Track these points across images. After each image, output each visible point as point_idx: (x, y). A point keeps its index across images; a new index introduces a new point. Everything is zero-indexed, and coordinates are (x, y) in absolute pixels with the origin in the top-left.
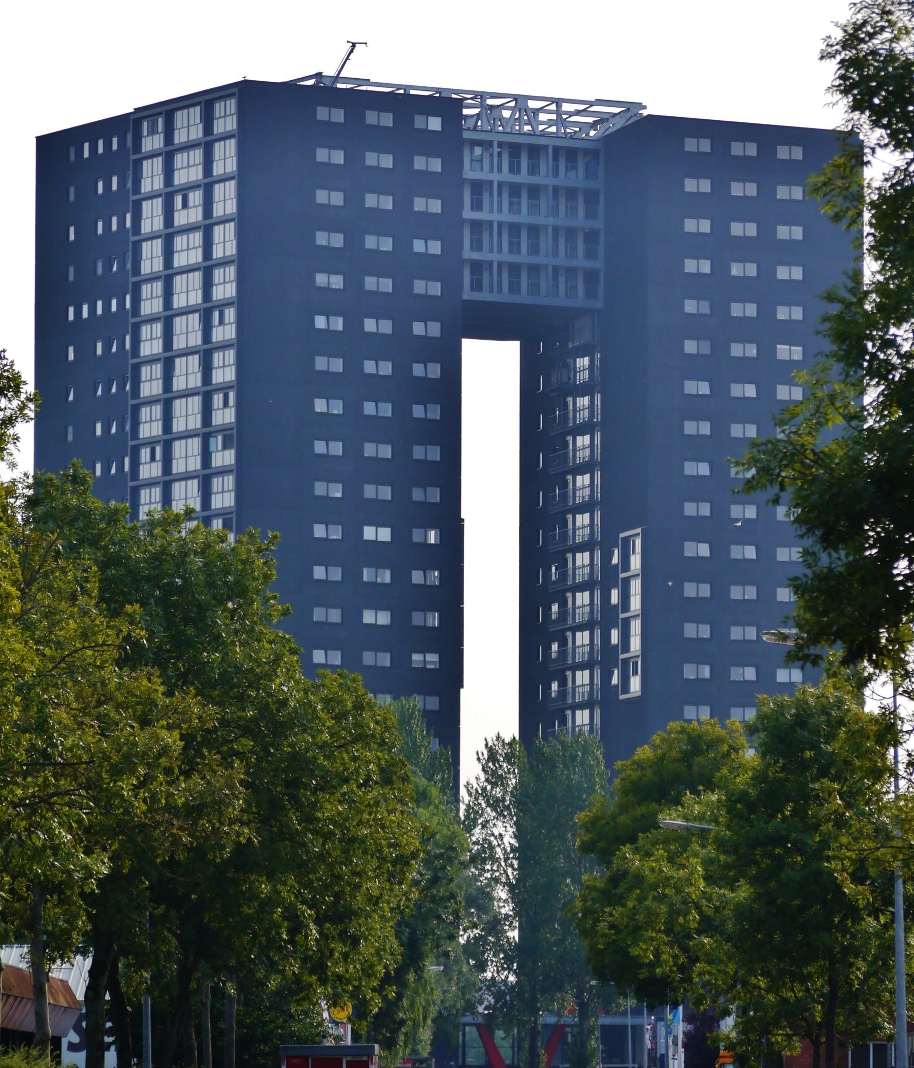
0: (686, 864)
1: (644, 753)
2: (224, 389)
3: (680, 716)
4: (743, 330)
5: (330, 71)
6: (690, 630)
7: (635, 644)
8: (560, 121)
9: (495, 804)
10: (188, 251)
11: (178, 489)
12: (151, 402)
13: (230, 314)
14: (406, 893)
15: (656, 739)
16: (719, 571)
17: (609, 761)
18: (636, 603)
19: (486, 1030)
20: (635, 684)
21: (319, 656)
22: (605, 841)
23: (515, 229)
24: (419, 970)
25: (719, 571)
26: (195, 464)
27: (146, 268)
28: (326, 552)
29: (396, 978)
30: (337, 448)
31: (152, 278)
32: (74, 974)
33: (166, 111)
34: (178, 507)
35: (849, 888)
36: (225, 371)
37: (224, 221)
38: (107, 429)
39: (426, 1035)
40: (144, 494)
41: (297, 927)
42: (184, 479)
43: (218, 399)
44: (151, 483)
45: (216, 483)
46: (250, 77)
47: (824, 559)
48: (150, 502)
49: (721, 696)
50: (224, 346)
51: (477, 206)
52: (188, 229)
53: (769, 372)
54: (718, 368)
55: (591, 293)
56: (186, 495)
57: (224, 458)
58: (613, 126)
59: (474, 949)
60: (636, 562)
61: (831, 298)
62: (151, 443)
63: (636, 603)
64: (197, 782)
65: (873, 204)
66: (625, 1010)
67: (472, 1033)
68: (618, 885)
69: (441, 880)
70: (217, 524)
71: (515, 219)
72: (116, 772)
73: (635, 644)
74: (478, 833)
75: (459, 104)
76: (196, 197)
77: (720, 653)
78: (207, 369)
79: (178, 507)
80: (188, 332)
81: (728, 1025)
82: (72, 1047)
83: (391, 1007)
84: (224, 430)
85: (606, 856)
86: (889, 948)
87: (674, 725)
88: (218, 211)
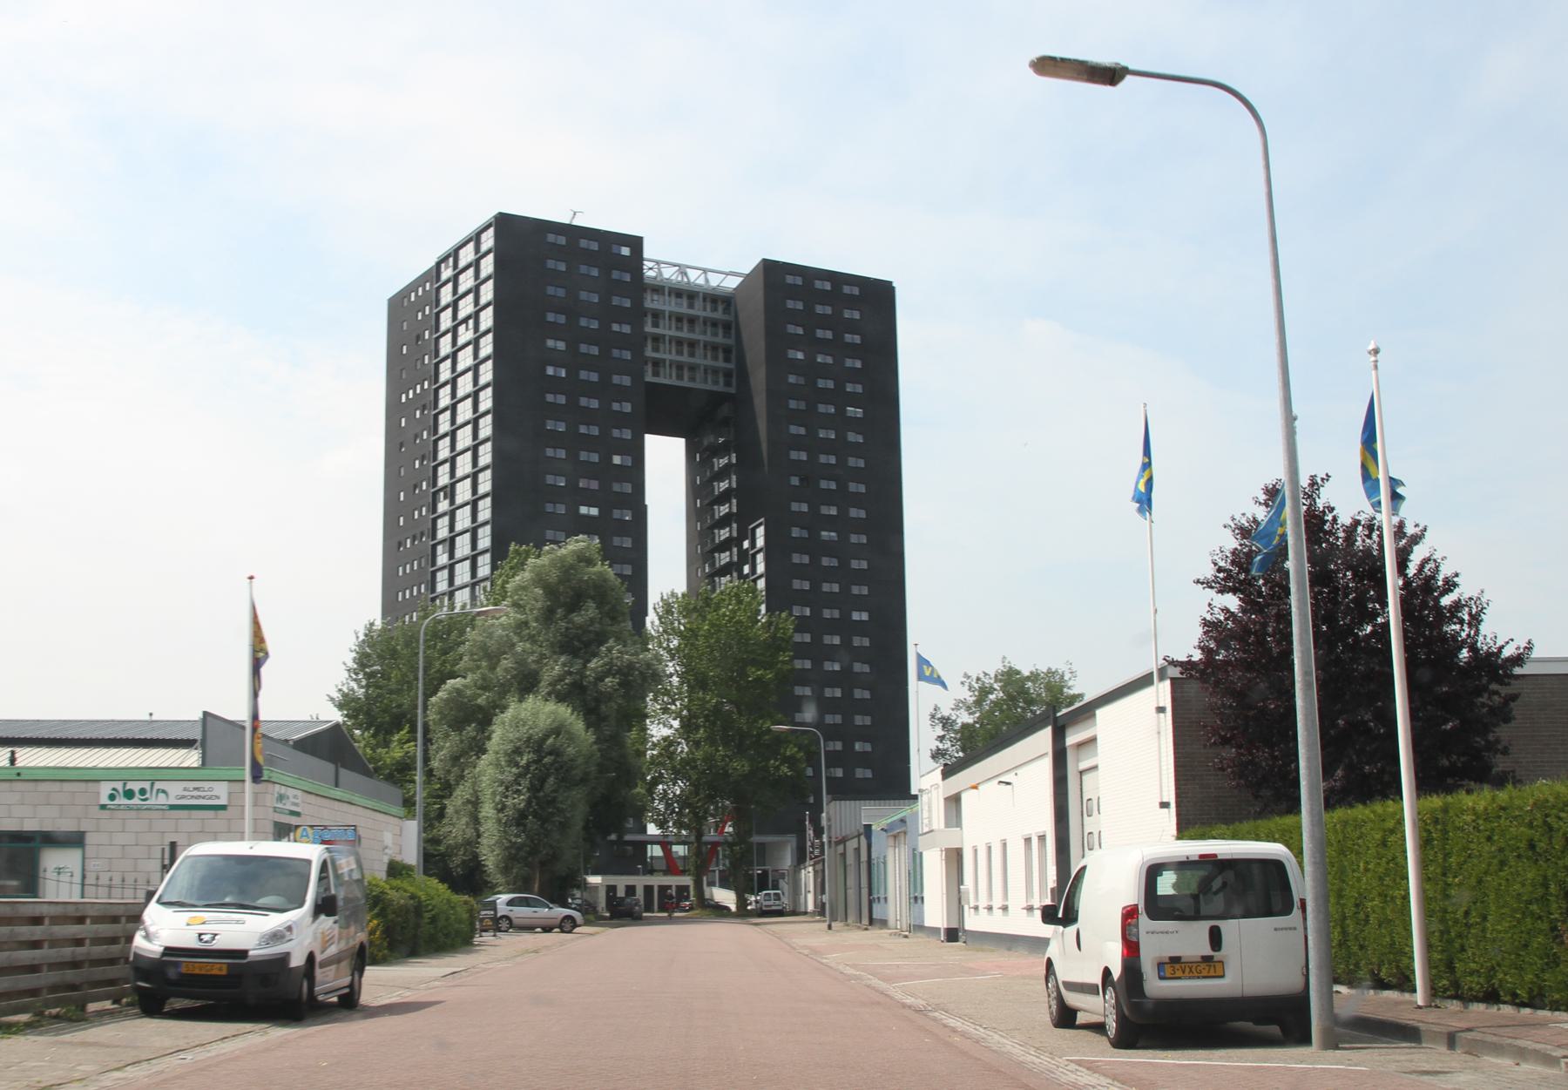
4: (825, 396)
6: (797, 584)
55: (728, 384)
71: (679, 334)
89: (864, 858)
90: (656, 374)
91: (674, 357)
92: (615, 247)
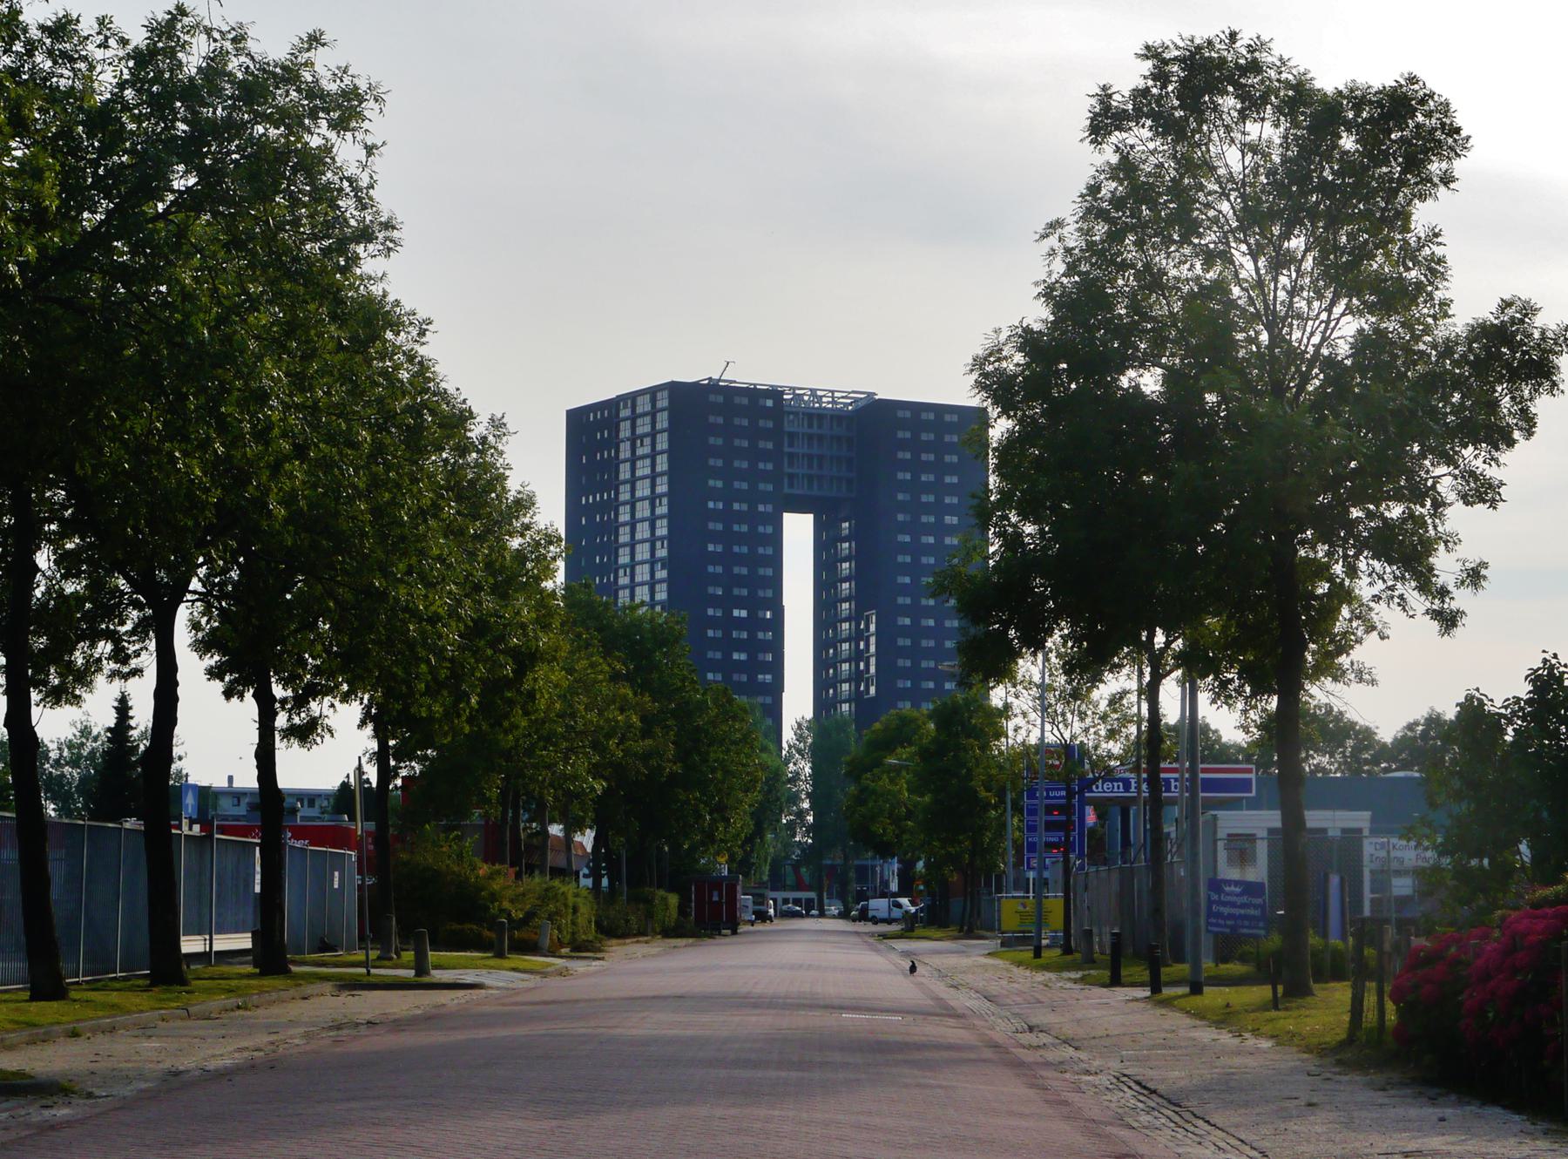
0: (899, 779)
1: (877, 726)
2: (662, 538)
3: (895, 707)
5: (716, 377)
7: (873, 669)
8: (834, 402)
9: (799, 751)
10: (643, 469)
11: (638, 590)
12: (624, 545)
13: (665, 501)
14: (756, 796)
15: (883, 719)
16: (915, 632)
17: (858, 729)
18: (873, 649)
19: (796, 867)
20: (873, 690)
21: (710, 676)
22: (857, 770)
23: (810, 457)
24: (762, 838)
25: (915, 632)
26: (647, 577)
27: (622, 477)
28: (713, 623)
29: (749, 840)
30: (719, 569)
31: (625, 482)
32: (587, 839)
33: (633, 397)
34: (637, 600)
35: (983, 794)
36: (662, 530)
37: (662, 453)
38: (602, 559)
39: (766, 869)
40: (621, 593)
41: (700, 817)
42: (642, 586)
43: (658, 544)
44: (624, 587)
45: (658, 587)
46: (887, 391)
47: (972, 631)
48: (624, 596)
49: (916, 696)
50: (661, 517)
51: (791, 445)
52: (643, 457)
53: (941, 530)
54: (916, 529)
56: (642, 594)
57: (661, 574)
58: (860, 404)
59: (791, 826)
60: (873, 628)
61: (974, 496)
62: (624, 566)
63: (873, 649)
64: (649, 742)
65: (995, 449)
66: (868, 858)
67: (789, 869)
68: (861, 798)
69: (775, 786)
70: (658, 608)
72: (609, 736)
73: (873, 669)
74: (791, 767)
75: (783, 393)
76: (647, 441)
77: (916, 674)
78: (653, 528)
79: (637, 600)
80: (643, 510)
81: (920, 865)
82: (585, 876)
83: (748, 855)
84: (661, 559)
85: (857, 779)
86: (1003, 826)
87: (893, 711)
88: (659, 447)
89: (965, 1055)
90: (791, 485)
91: (806, 450)
92: (761, 402)
